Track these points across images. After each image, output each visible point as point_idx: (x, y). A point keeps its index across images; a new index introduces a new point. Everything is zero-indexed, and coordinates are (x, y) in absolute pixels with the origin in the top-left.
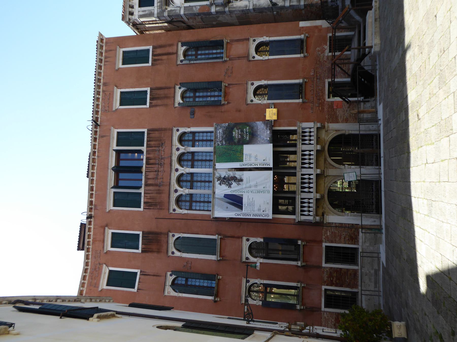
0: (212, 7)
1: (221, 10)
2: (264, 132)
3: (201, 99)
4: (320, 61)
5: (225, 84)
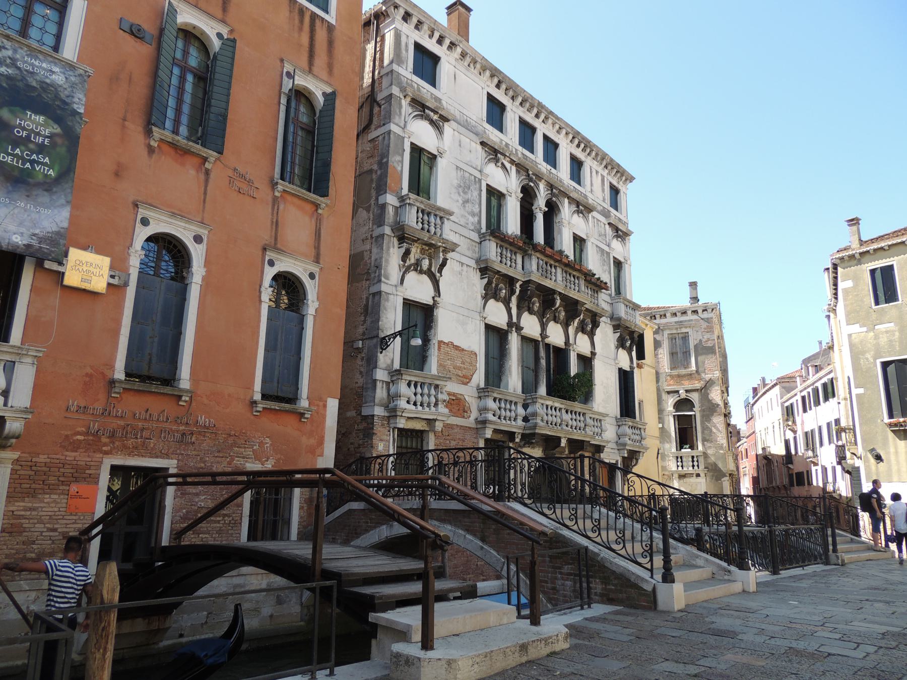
0: (395, 199)
1: (387, 217)
2: (21, 224)
3: (175, 81)
4: (235, 444)
5: (212, 159)
